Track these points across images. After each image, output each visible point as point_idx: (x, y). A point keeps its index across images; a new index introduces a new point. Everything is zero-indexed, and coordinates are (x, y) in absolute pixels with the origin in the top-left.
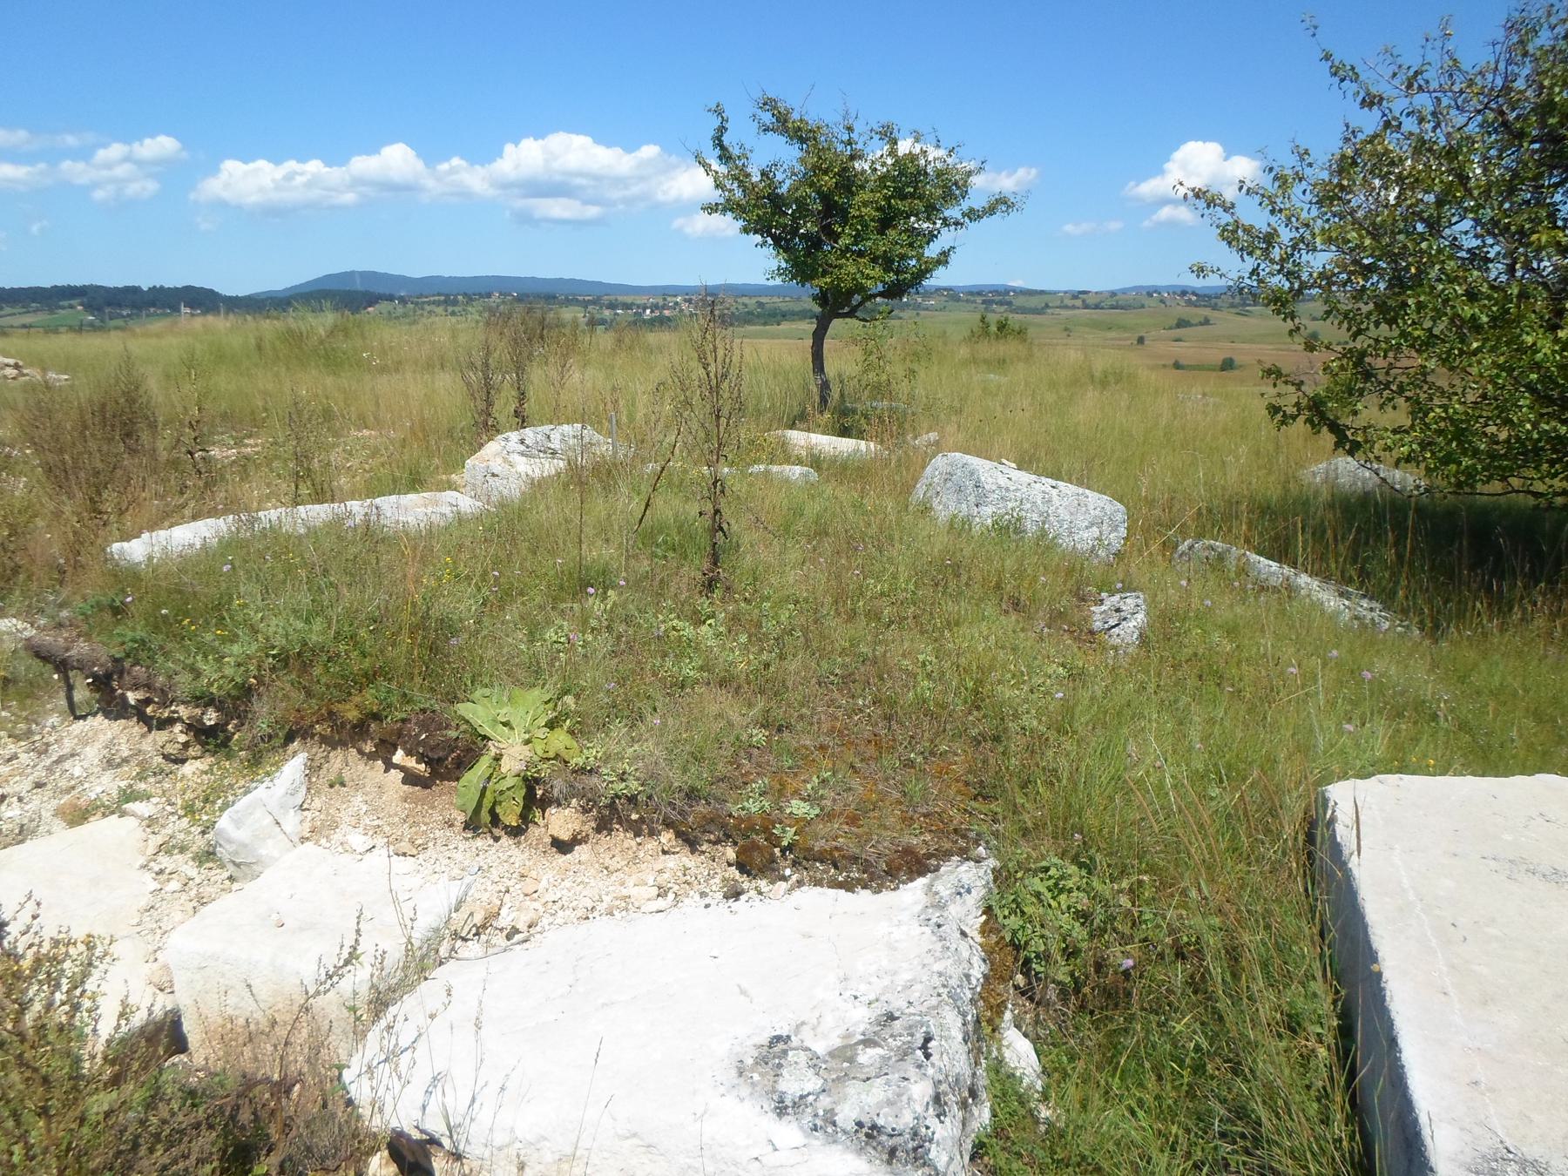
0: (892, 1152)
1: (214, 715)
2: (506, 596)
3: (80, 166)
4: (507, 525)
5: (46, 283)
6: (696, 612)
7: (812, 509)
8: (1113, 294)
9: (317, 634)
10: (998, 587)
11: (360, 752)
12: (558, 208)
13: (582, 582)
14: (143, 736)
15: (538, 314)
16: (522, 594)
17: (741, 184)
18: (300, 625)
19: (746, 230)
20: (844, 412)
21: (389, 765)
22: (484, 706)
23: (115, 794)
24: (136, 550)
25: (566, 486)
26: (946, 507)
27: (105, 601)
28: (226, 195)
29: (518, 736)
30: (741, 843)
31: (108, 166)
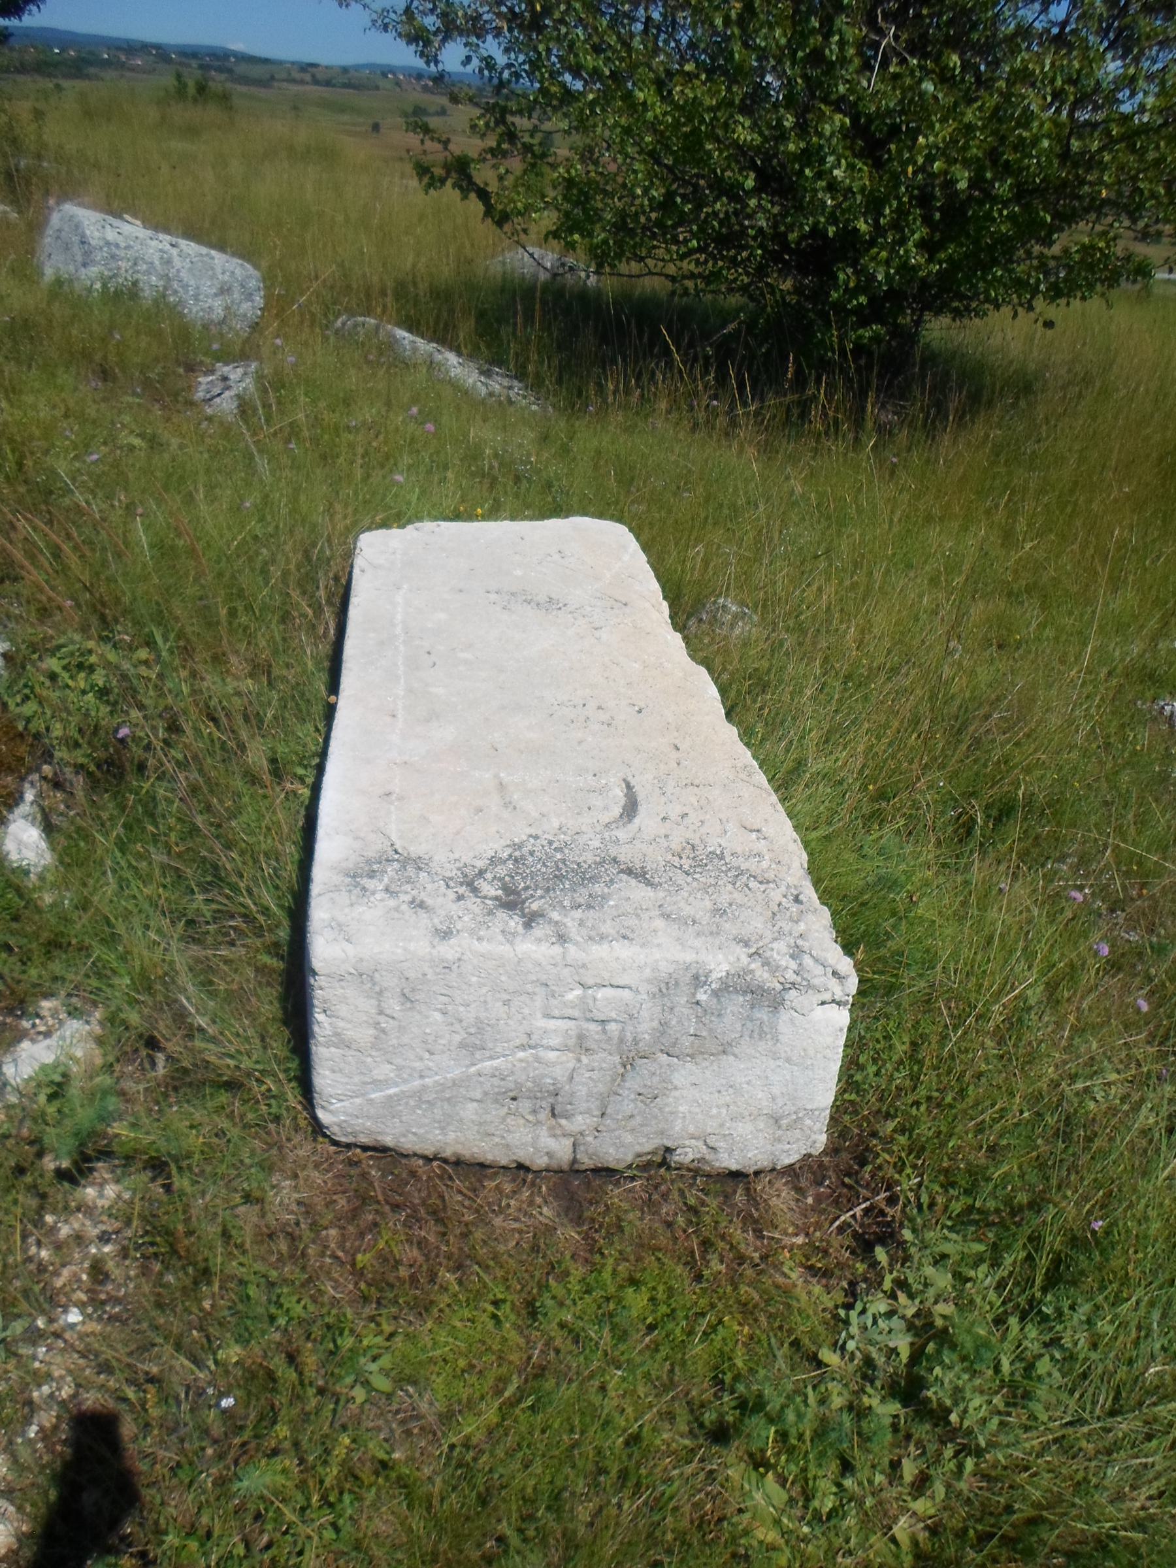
8: (345, 70)
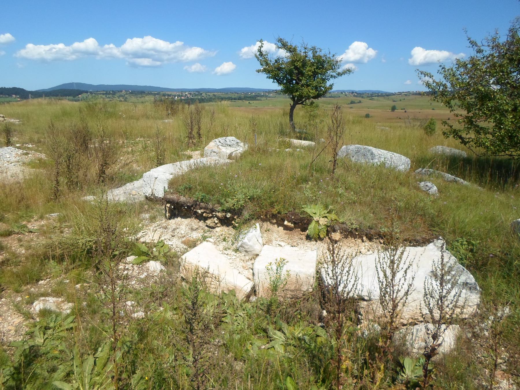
0: (470, 288)
12: (146, 62)
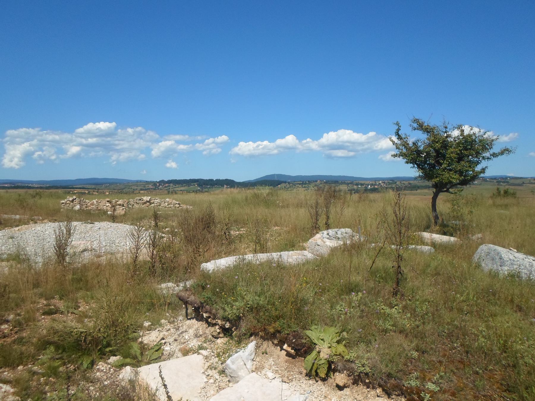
1: (229, 325)
2: (324, 291)
3: (201, 145)
4: (322, 264)
5: (188, 178)
6: (390, 303)
7: (434, 264)
9: (262, 301)
10: (512, 301)
11: (273, 343)
12: (340, 153)
13: (351, 289)
14: (207, 328)
15: (333, 188)
16: (328, 291)
17: (405, 147)
18: (257, 298)
19: (407, 163)
20: (444, 225)
21: (282, 349)
22: (315, 332)
23: (197, 346)
24: (210, 266)
25: (344, 251)
26: (487, 266)
27: (200, 284)
28: (239, 152)
29: (326, 345)
30: (408, 397)
31: (208, 145)
